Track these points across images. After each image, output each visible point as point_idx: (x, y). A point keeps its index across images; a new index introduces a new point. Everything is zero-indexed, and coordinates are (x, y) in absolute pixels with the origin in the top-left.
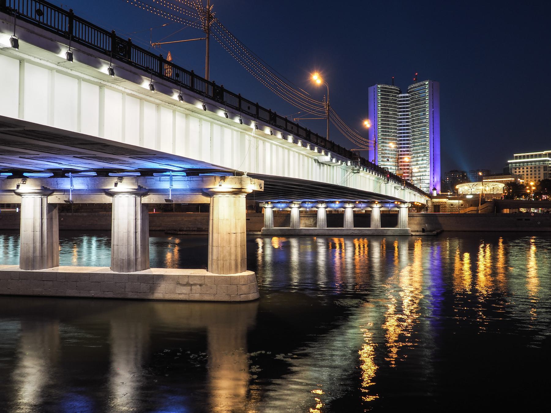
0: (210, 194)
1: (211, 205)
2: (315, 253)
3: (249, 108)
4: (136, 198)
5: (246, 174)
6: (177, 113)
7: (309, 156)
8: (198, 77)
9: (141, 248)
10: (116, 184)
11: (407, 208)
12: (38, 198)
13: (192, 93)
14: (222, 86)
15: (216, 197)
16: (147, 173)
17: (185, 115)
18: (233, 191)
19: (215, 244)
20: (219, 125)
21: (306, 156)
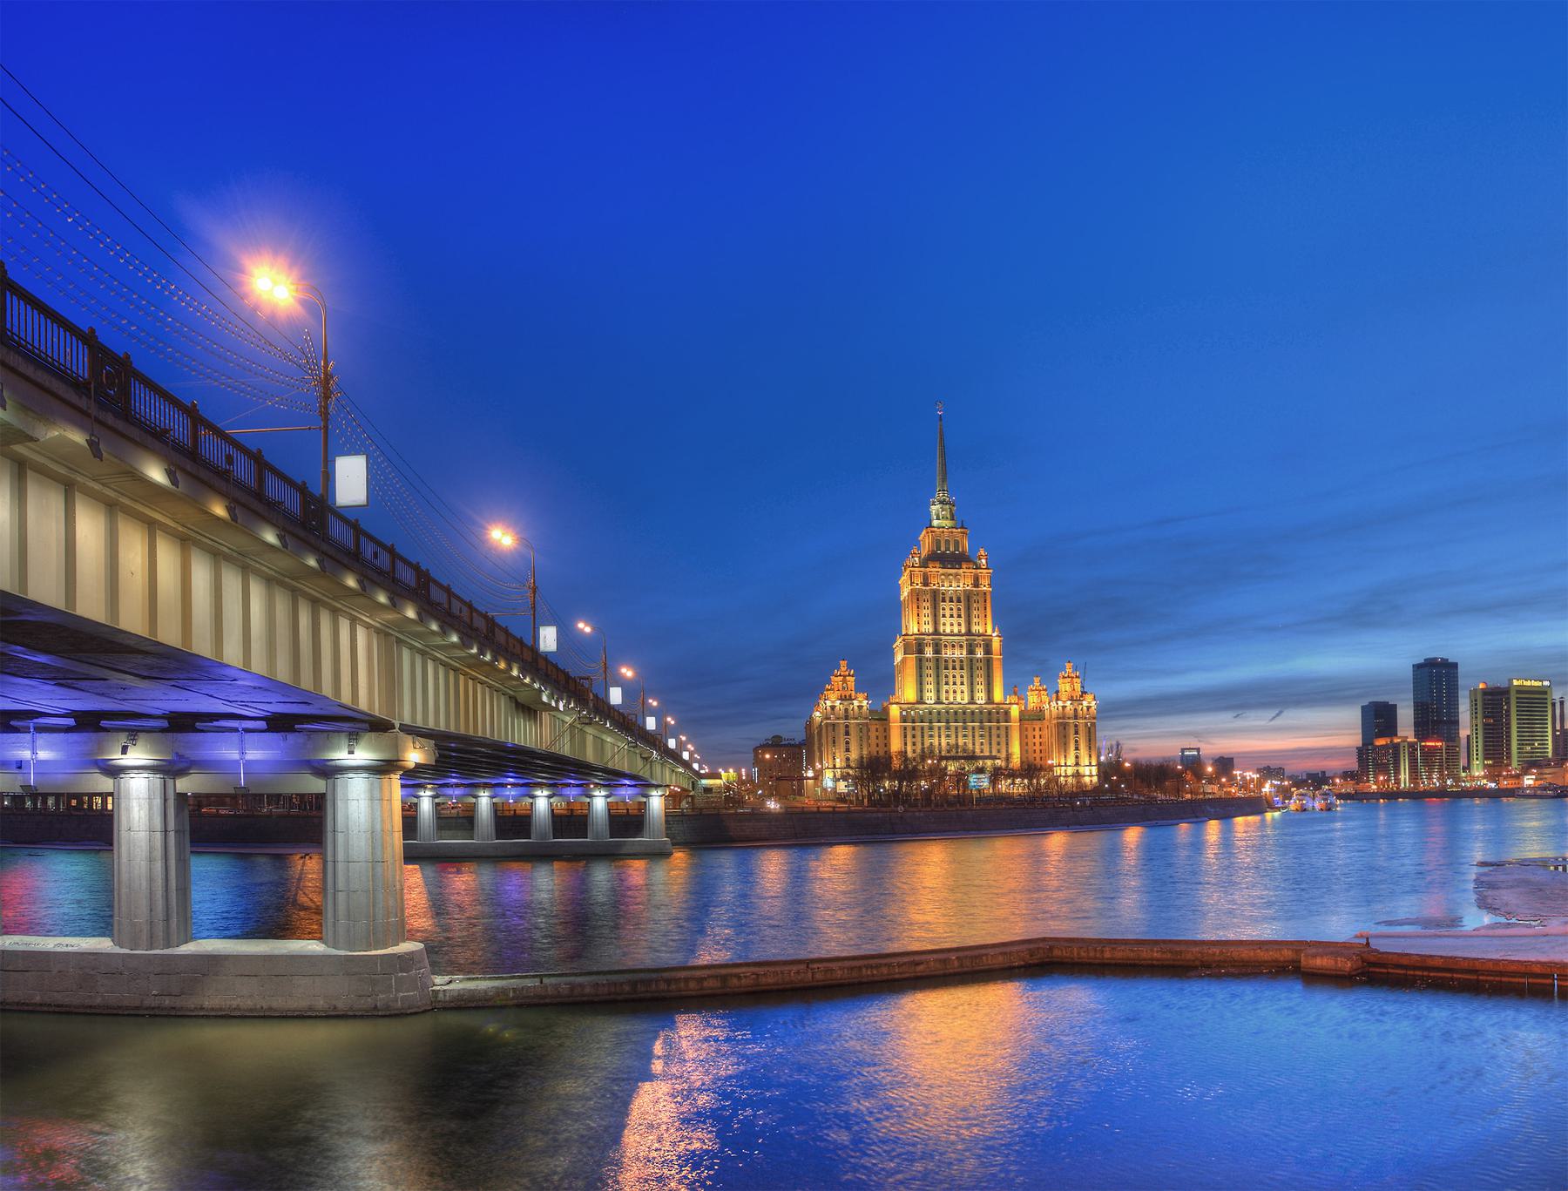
0: (330, 772)
1: (329, 797)
2: (676, 780)
3: (376, 555)
4: (165, 781)
5: (397, 726)
6: (29, 473)
7: (450, 665)
8: (477, 611)
9: (177, 906)
10: (124, 750)
11: (661, 796)
12: (157, 780)
13: (256, 505)
14: (393, 545)
15: (341, 780)
16: (182, 723)
17: (17, 465)
18: (154, 766)
19: (341, 884)
20: (59, 483)
21: (445, 665)
